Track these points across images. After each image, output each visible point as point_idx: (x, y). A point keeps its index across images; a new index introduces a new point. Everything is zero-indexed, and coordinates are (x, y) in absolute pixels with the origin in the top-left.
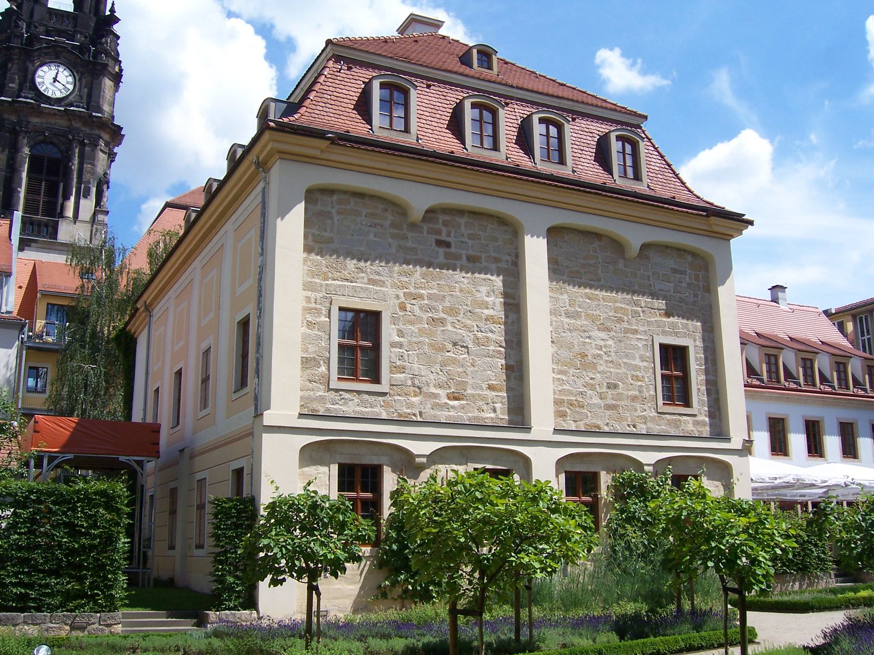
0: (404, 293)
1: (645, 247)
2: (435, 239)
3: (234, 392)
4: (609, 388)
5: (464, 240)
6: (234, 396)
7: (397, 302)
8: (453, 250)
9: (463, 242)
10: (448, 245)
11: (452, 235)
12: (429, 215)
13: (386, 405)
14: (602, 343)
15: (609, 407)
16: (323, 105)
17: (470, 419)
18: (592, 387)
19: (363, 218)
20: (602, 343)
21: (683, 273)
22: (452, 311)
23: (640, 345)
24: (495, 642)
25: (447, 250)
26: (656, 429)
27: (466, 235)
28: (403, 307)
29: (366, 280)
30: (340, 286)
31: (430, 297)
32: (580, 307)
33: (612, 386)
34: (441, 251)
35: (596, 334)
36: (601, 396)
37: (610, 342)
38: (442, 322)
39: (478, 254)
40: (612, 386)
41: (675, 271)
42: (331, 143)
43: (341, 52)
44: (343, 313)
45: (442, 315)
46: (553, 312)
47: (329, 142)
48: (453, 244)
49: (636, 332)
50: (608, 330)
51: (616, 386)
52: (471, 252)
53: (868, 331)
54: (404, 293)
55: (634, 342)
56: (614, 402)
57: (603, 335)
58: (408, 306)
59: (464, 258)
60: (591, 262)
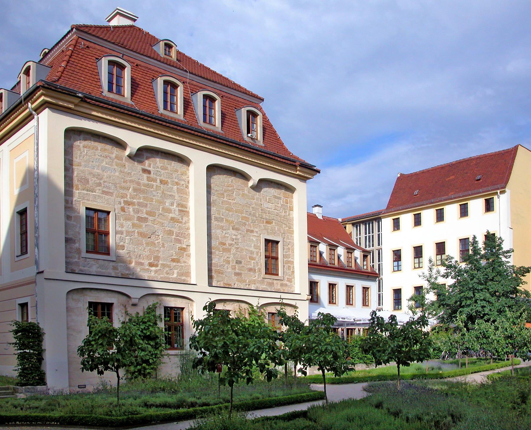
0: (124, 201)
1: (261, 181)
2: (142, 168)
3: (17, 256)
4: (237, 263)
5: (158, 170)
6: (17, 259)
7: (120, 206)
8: (152, 175)
9: (157, 171)
10: (149, 172)
11: (152, 166)
12: (140, 152)
13: (115, 268)
14: (234, 237)
15: (237, 274)
16: (72, 72)
17: (161, 278)
18: (228, 262)
19: (99, 151)
20: (234, 237)
21: (279, 198)
22: (150, 213)
23: (254, 239)
24: (20, 349)
25: (148, 175)
26: (264, 287)
27: (160, 167)
28: (123, 209)
29: (101, 192)
30: (87, 194)
31: (139, 204)
32: (222, 215)
34: (145, 176)
35: (231, 231)
37: (239, 237)
38: (145, 220)
39: (167, 179)
40: (239, 262)
41: (275, 197)
42: (81, 101)
43: (87, 37)
44: (88, 211)
45: (145, 216)
46: (293, 262)
47: (80, 99)
48: (152, 173)
49: (252, 231)
50: (237, 229)
51: (240, 262)
52: (163, 178)
53: (360, 234)
54: (124, 201)
55: (252, 238)
56: (240, 271)
58: (126, 209)
59: (158, 181)
60: (230, 188)
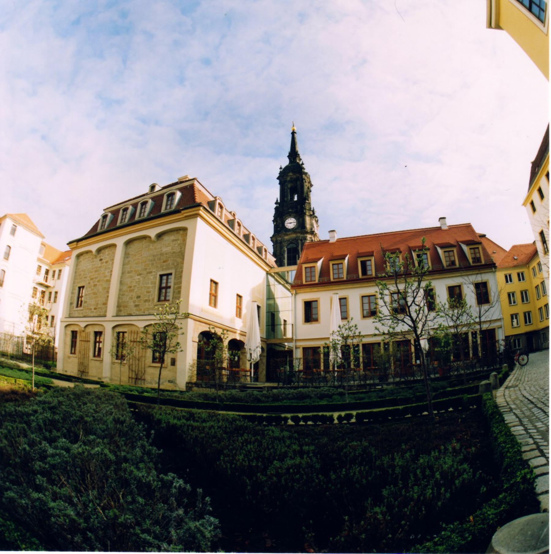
21: (178, 240)
33: (138, 297)
36: (134, 302)
41: (173, 241)
57: (139, 277)
